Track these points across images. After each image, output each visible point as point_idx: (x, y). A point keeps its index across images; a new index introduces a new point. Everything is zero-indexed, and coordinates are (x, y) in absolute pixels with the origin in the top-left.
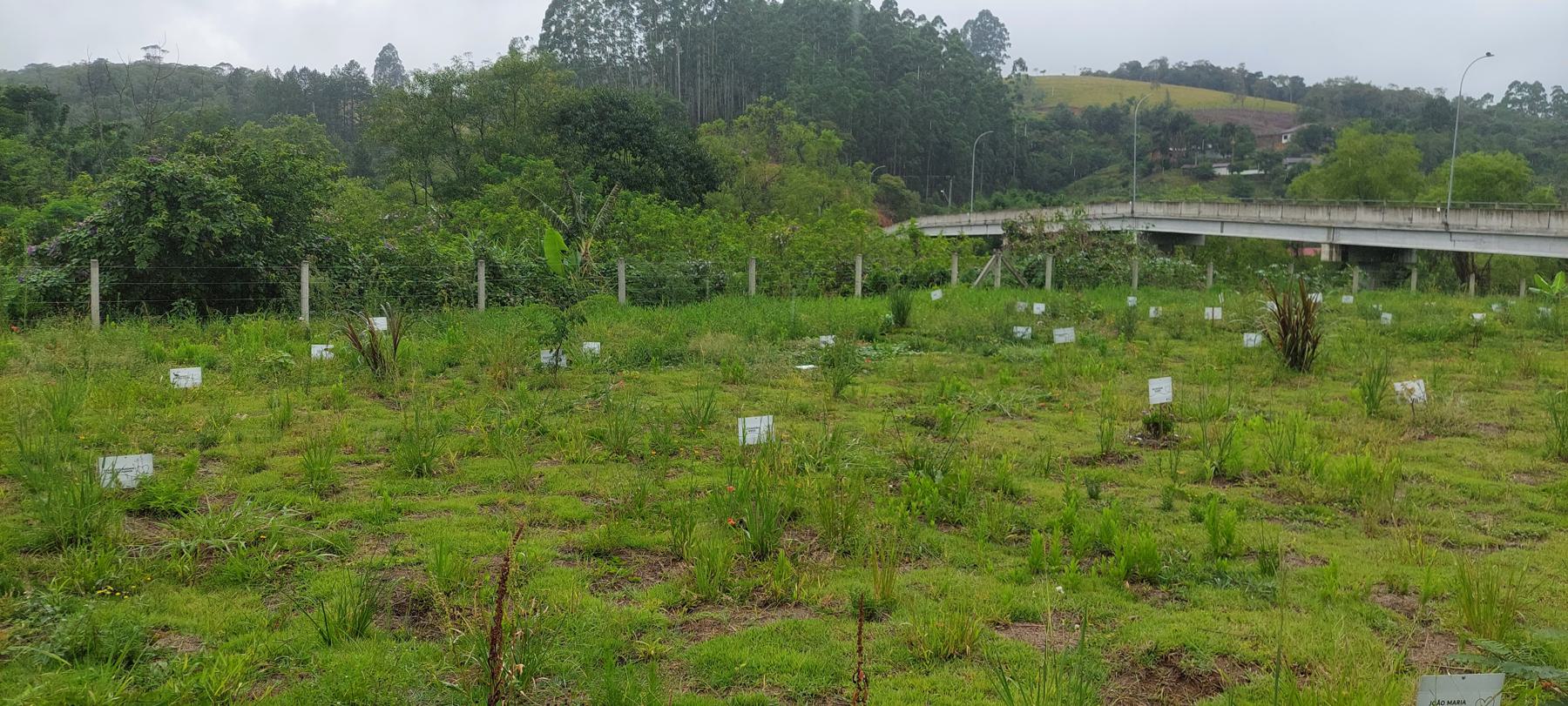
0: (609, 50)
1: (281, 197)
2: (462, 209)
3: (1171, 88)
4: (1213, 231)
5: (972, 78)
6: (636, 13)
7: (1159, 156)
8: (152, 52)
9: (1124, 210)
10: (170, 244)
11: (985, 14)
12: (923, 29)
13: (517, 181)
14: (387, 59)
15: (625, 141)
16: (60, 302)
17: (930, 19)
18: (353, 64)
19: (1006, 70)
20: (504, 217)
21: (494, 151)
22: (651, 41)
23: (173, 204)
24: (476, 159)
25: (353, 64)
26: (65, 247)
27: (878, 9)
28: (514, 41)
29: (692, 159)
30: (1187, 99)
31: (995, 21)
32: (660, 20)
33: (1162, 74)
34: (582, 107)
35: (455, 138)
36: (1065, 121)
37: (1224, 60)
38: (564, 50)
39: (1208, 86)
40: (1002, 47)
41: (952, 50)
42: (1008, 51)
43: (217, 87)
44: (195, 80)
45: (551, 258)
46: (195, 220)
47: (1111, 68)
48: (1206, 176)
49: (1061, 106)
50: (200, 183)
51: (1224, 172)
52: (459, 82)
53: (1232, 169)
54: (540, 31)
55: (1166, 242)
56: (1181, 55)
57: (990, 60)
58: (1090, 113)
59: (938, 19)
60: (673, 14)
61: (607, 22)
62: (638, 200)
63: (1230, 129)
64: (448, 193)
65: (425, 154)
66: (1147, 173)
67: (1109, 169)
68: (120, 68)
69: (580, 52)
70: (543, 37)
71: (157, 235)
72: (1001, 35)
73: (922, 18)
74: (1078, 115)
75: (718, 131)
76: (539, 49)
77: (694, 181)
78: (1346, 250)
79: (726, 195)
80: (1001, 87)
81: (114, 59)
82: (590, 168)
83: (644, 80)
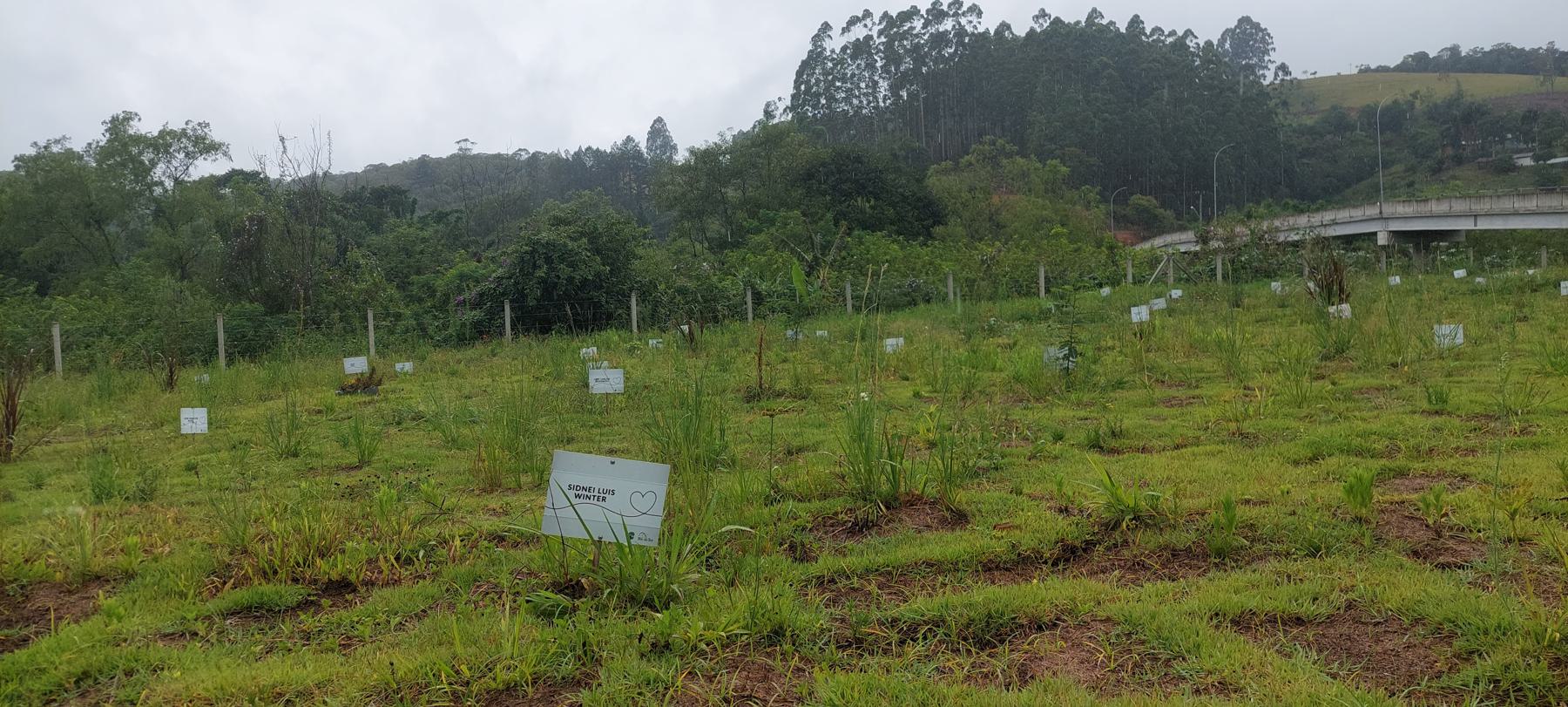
0: (855, 101)
1: (612, 250)
2: (733, 256)
3: (1461, 76)
4: (1465, 225)
5: (1230, 89)
6: (879, 64)
7: (1450, 151)
8: (463, 145)
9: (1372, 211)
10: (548, 287)
11: (1245, 20)
12: (1173, 45)
13: (773, 230)
14: (658, 131)
15: (861, 189)
16: (483, 331)
17: (1180, 33)
18: (629, 139)
19: (1269, 77)
20: (763, 259)
21: (753, 207)
22: (894, 89)
23: (549, 260)
24: (740, 215)
25: (629, 139)
26: (481, 295)
27: (1123, 30)
28: (768, 105)
29: (919, 199)
30: (1480, 87)
31: (1257, 26)
32: (902, 68)
33: (1454, 62)
34: (823, 164)
35: (724, 200)
36: (1339, 123)
37: (1528, 39)
38: (814, 107)
39: (1511, 70)
40: (1266, 52)
41: (1206, 62)
42: (1273, 56)
43: (517, 170)
44: (501, 165)
45: (798, 286)
46: (564, 270)
47: (1393, 61)
48: (1506, 168)
49: (1334, 108)
50: (565, 245)
51: (1527, 162)
52: (724, 153)
53: (1536, 158)
54: (792, 91)
55: (1424, 240)
56: (1476, 38)
57: (1250, 69)
58: (1368, 112)
59: (1188, 33)
60: (914, 60)
61: (853, 75)
62: (869, 238)
63: (1531, 116)
64: (719, 245)
65: (700, 214)
66: (1437, 170)
67: (1393, 169)
68: (439, 161)
69: (829, 107)
70: (793, 97)
71: (542, 281)
72: (1263, 40)
73: (1173, 33)
74: (1354, 115)
75: (946, 172)
76: (792, 108)
77: (921, 218)
78: (1396, 234)
79: (955, 227)
80: (1263, 94)
81: (435, 154)
82: (829, 216)
83: (890, 127)
